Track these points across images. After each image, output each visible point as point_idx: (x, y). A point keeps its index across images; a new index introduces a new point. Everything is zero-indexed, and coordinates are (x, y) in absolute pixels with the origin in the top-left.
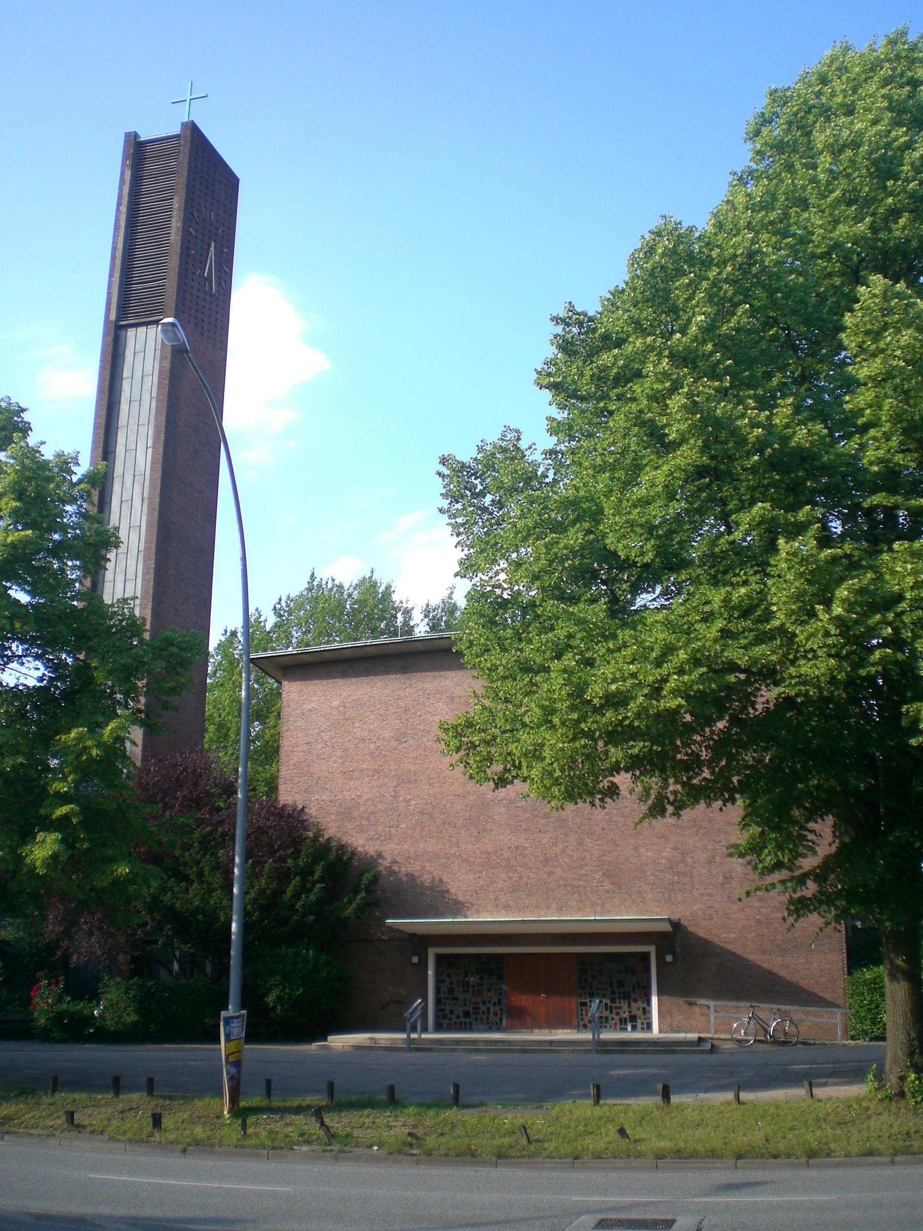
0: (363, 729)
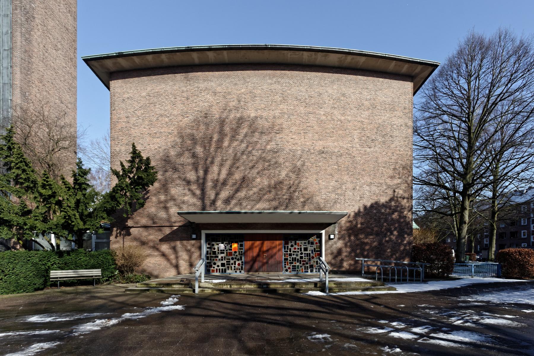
0: (161, 110)
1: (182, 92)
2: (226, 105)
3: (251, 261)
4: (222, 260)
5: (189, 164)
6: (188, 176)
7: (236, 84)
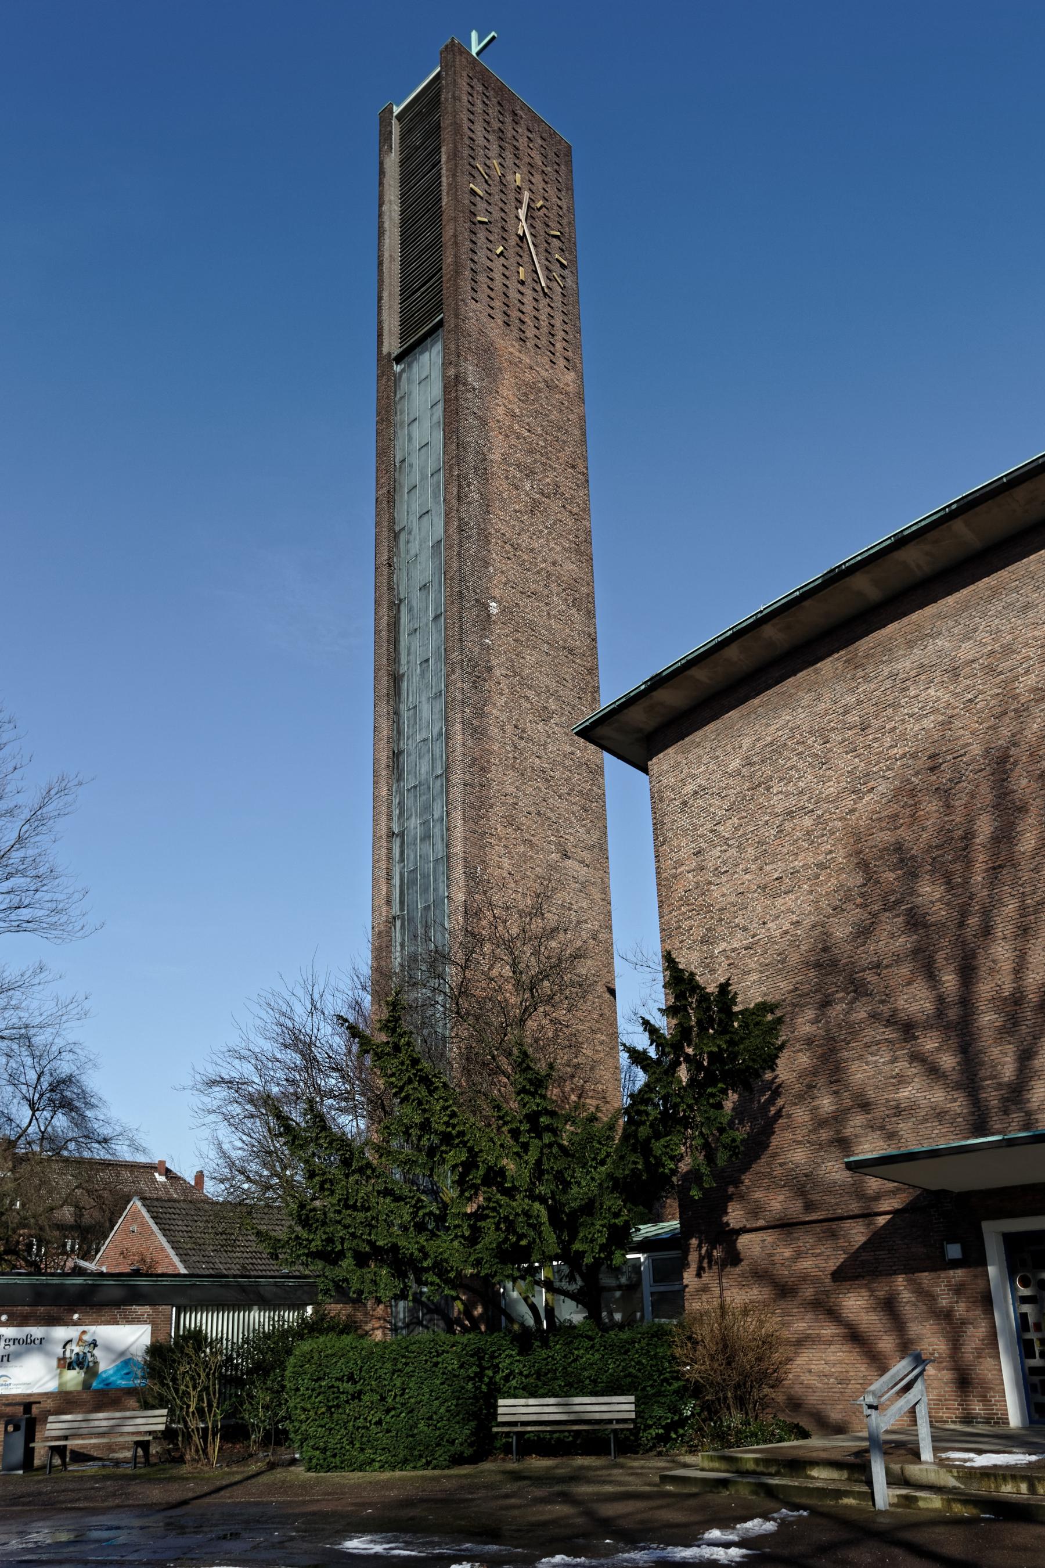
0: (787, 795)
1: (845, 713)
2: (1008, 695)
5: (898, 960)
6: (901, 1003)
7: (1027, 607)
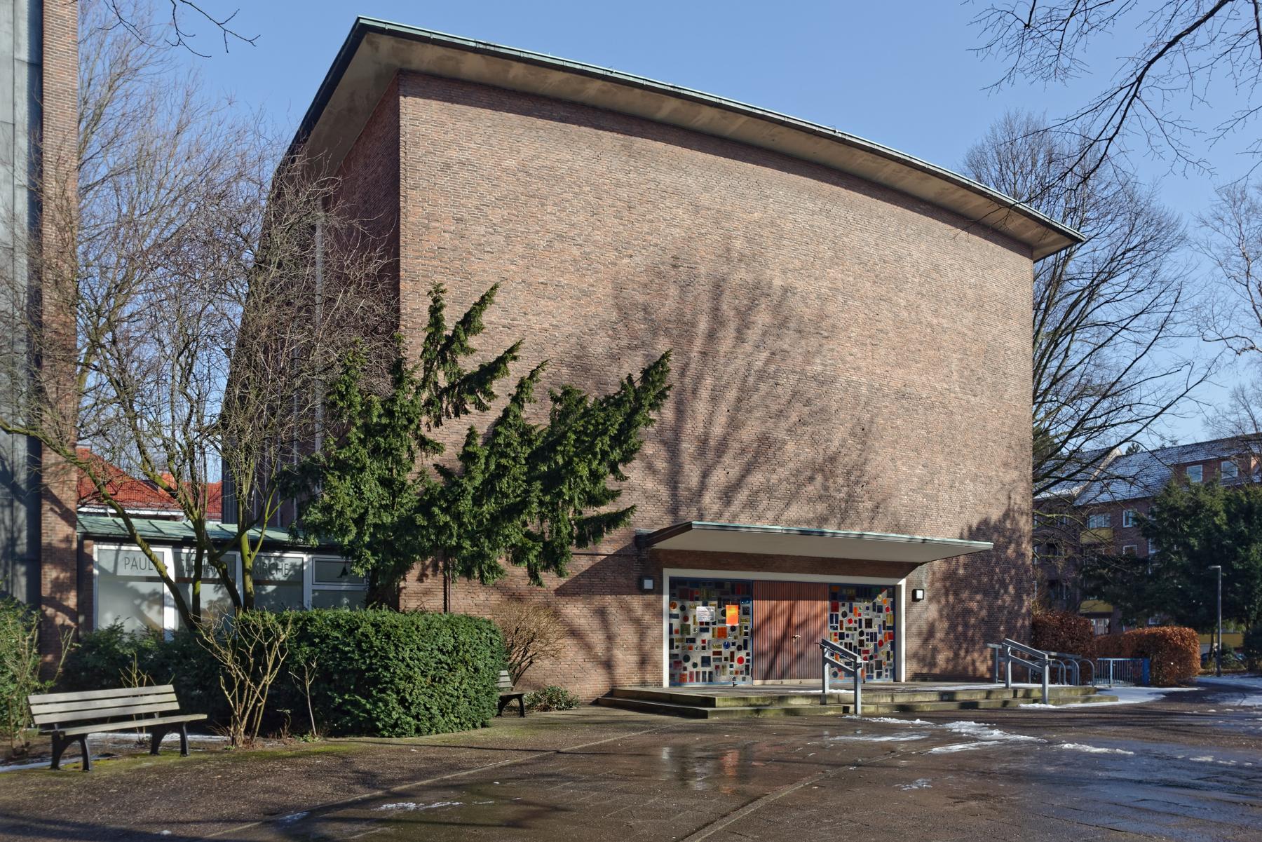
0: (560, 219)
1: (617, 186)
3: (771, 648)
4: (704, 648)
